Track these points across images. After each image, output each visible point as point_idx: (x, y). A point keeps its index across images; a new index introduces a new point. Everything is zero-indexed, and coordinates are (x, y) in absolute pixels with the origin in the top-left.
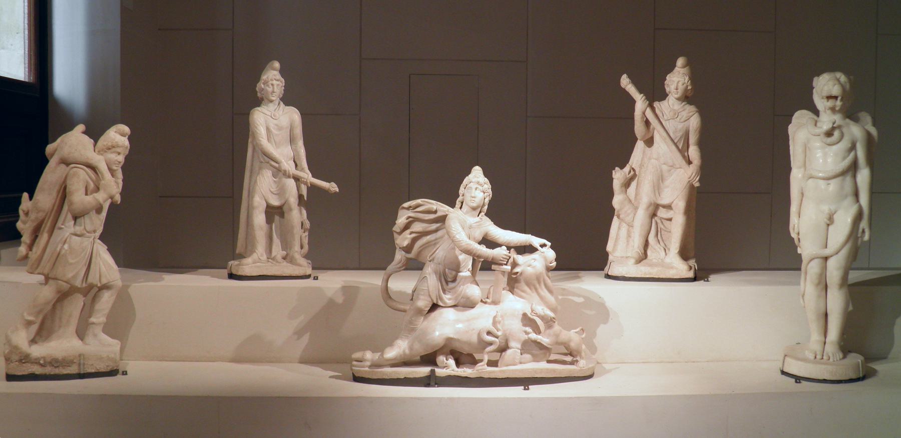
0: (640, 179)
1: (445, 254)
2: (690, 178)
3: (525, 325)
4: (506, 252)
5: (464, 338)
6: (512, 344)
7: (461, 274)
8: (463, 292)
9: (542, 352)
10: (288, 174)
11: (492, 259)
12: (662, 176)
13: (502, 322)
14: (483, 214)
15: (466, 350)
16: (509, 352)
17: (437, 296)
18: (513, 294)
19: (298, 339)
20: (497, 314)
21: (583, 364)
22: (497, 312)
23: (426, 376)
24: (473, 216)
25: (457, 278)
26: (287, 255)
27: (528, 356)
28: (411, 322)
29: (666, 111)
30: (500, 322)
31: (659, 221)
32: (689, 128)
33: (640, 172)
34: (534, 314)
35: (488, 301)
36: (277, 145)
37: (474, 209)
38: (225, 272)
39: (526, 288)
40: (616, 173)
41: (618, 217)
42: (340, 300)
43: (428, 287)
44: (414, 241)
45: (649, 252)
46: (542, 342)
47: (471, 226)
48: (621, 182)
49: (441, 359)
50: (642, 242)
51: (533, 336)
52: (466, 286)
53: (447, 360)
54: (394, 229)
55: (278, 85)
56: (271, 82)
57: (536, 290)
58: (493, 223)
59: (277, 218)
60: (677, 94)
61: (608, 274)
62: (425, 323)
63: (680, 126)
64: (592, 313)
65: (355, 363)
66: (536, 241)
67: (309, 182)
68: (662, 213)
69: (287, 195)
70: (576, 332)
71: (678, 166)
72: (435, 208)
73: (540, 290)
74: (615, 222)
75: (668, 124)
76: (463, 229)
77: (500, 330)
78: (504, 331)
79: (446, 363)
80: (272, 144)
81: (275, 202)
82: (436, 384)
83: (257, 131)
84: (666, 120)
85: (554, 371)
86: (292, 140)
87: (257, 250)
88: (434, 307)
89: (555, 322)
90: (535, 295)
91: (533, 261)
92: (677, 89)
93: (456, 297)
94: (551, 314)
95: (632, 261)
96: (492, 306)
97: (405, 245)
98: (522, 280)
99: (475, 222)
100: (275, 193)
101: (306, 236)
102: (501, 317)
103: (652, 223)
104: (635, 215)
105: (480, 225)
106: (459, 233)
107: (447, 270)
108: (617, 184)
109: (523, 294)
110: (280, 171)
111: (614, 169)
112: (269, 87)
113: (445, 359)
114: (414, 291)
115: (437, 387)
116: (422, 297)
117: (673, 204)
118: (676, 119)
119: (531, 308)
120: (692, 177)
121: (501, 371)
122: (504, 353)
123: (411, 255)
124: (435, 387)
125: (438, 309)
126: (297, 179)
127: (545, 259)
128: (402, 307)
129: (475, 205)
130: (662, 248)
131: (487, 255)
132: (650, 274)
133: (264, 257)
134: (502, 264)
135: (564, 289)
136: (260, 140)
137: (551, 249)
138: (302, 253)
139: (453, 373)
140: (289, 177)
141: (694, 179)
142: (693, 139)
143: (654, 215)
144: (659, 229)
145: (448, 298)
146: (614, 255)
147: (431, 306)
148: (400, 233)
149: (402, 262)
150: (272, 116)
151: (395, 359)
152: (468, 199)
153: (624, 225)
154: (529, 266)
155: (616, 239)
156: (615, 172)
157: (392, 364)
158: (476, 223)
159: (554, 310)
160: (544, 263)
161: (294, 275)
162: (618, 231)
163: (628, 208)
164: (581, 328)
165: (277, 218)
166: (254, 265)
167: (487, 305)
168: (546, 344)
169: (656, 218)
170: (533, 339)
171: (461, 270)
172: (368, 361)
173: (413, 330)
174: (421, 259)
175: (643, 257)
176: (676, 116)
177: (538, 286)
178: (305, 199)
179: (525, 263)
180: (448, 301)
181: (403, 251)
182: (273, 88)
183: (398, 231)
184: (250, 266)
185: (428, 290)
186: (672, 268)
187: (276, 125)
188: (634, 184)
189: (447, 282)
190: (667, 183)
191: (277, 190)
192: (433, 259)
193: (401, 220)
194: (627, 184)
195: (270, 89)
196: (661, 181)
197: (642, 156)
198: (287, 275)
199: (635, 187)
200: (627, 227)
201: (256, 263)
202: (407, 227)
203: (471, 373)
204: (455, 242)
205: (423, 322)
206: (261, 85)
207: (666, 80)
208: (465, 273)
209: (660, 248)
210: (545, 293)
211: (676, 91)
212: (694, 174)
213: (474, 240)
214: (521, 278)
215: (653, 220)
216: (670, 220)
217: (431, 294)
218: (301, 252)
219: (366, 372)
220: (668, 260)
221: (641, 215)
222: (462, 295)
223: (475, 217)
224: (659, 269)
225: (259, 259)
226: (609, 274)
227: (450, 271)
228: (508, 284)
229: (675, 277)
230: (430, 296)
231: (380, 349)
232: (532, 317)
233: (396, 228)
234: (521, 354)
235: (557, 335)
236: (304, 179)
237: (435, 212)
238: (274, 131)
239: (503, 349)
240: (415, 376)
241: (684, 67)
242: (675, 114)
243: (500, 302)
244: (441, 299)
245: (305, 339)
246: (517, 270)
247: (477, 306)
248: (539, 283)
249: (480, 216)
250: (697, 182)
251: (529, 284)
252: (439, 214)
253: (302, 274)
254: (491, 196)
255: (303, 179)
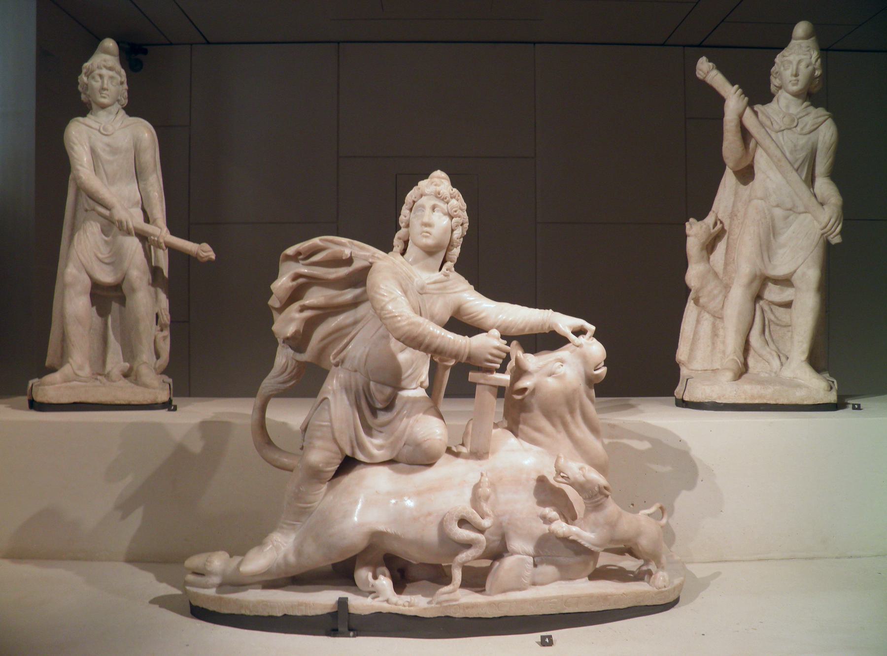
0: (731, 237)
1: (367, 349)
2: (826, 227)
3: (542, 503)
4: (502, 343)
5: (410, 532)
6: (515, 544)
7: (405, 393)
8: (407, 433)
9: (579, 559)
10: (125, 228)
11: (469, 358)
12: (774, 227)
13: (492, 497)
14: (449, 264)
15: (415, 556)
16: (508, 562)
17: (351, 442)
18: (516, 435)
19: (123, 517)
20: (480, 481)
21: (664, 581)
22: (482, 475)
23: (329, 614)
24: (428, 268)
25: (397, 402)
26: (131, 369)
27: (549, 570)
28: (298, 496)
29: (776, 118)
30: (487, 498)
31: (766, 308)
32: (817, 145)
33: (730, 225)
34: (564, 480)
35: (464, 450)
36: (111, 180)
37: (430, 252)
38: (24, 400)
39: (544, 423)
40: (691, 227)
41: (697, 301)
42: (196, 446)
43: (331, 421)
44: (310, 325)
45: (751, 362)
46: (580, 541)
47: (423, 288)
48: (702, 241)
49: (363, 574)
50: (740, 341)
51: (561, 527)
52: (414, 417)
53: (375, 577)
54: (270, 303)
55: (111, 78)
56: (97, 72)
57: (565, 425)
58: (472, 287)
59: (115, 306)
60: (796, 84)
61: (683, 401)
62: (330, 498)
63: (802, 141)
64: (668, 469)
65: (190, 577)
66: (564, 323)
67: (161, 241)
68: (773, 293)
69: (126, 264)
70: (649, 515)
71: (801, 209)
72: (347, 252)
73: (573, 427)
74: (690, 312)
75: (781, 138)
76: (405, 292)
77: (488, 515)
78: (497, 516)
79: (373, 586)
80: (101, 179)
81: (106, 277)
82: (350, 630)
83: (73, 154)
84: (777, 132)
85: (605, 598)
86: (139, 174)
87: (72, 358)
88: (348, 464)
89: (607, 496)
90: (562, 437)
91: (559, 364)
92: (796, 75)
93: (392, 443)
94: (596, 477)
95: (729, 375)
96: (472, 463)
97: (288, 335)
98: (536, 407)
99: (432, 280)
100: (106, 261)
101: (164, 338)
102: (489, 487)
103: (755, 310)
104: (725, 297)
105: (445, 288)
106: (394, 300)
107: (372, 384)
108: (693, 245)
109: (536, 435)
110: (113, 223)
111: (688, 221)
112: (97, 81)
113: (370, 575)
114: (305, 429)
115: (354, 636)
116: (319, 443)
117: (793, 277)
118: (794, 129)
119: (556, 466)
120: (828, 227)
121: (491, 604)
122: (497, 564)
123: (305, 357)
124: (349, 636)
125: (358, 467)
126: (143, 238)
127: (584, 359)
128: (285, 460)
129: (430, 241)
130: (775, 354)
131: (456, 348)
132: (760, 397)
133: (86, 371)
134: (490, 370)
135: (613, 426)
136: (78, 170)
137: (595, 340)
138: (157, 366)
139: (386, 607)
140: (128, 233)
141: (833, 229)
142: (822, 165)
143: (758, 297)
144: (767, 322)
145: (376, 446)
146: (691, 367)
147: (340, 462)
148: (281, 310)
149: (289, 370)
150: (102, 129)
151: (267, 572)
152: (416, 229)
153: (706, 316)
154: (550, 375)
155: (693, 339)
156: (691, 224)
157: (266, 581)
158: (435, 283)
159: (601, 469)
160: (582, 369)
161: (136, 403)
162: (696, 327)
163: (712, 286)
164: (658, 505)
165: (115, 306)
166: (64, 385)
167: (460, 461)
168: (590, 543)
169: (761, 302)
170: (561, 535)
171: (404, 384)
172: (216, 574)
173: (303, 512)
174: (324, 365)
175: (743, 371)
176: (795, 124)
177: (568, 418)
178: (166, 273)
179: (541, 368)
180: (375, 452)
181: (290, 347)
182: (103, 82)
183: (277, 305)
184: (57, 385)
185: (332, 427)
186: (799, 386)
187: (108, 145)
188: (721, 246)
189: (374, 411)
190: (783, 239)
191: (110, 257)
192: (343, 361)
193: (282, 283)
194: (710, 246)
195: (97, 84)
196: (772, 236)
197: (732, 200)
198: (123, 402)
199: (724, 252)
200: (712, 319)
201: (70, 381)
202: (296, 295)
203: (425, 609)
204: (386, 318)
205: (326, 495)
206: (83, 78)
207: (773, 64)
208: (414, 392)
209: (771, 353)
210: (582, 432)
211: (794, 78)
212: (833, 220)
213: (432, 318)
214: (533, 401)
215: (758, 306)
216: (788, 305)
217: (337, 435)
218: (155, 364)
219: (208, 598)
220: (787, 373)
221: (738, 296)
222: (405, 438)
223: (433, 271)
224: (777, 388)
225: (76, 375)
226: (686, 399)
227: (379, 386)
228: (506, 415)
229: (805, 403)
230: (335, 441)
231: (239, 550)
232: (557, 485)
233: (274, 302)
234: (535, 565)
235: (612, 525)
236: (154, 236)
237: (349, 261)
238: (105, 156)
239: (498, 553)
240: (304, 613)
241: (807, 37)
242: (793, 120)
243: (487, 453)
244: (362, 447)
245: (136, 517)
246: (526, 383)
247: (440, 462)
248: (572, 412)
249: (444, 269)
250: (837, 235)
251: (549, 414)
252: (357, 264)
253: (149, 402)
254: (466, 225)
255: (152, 237)
